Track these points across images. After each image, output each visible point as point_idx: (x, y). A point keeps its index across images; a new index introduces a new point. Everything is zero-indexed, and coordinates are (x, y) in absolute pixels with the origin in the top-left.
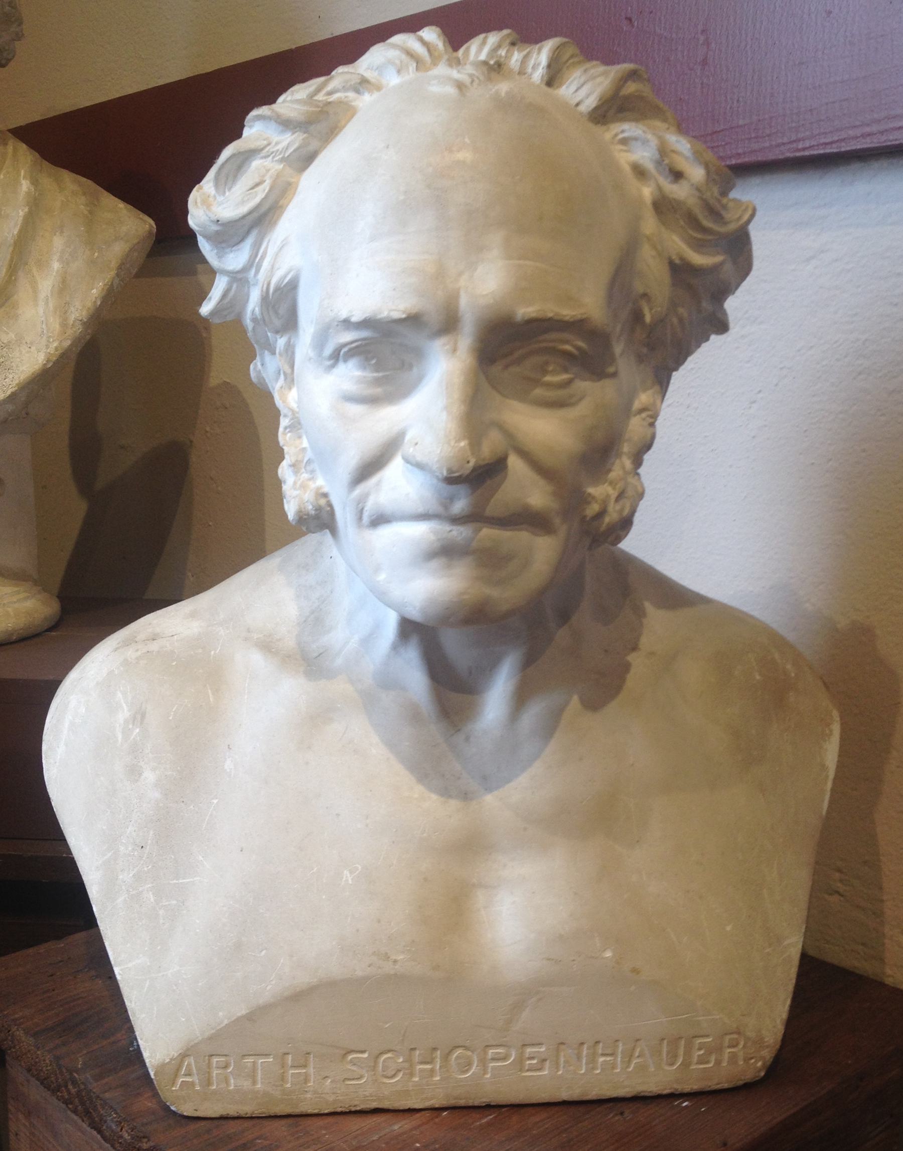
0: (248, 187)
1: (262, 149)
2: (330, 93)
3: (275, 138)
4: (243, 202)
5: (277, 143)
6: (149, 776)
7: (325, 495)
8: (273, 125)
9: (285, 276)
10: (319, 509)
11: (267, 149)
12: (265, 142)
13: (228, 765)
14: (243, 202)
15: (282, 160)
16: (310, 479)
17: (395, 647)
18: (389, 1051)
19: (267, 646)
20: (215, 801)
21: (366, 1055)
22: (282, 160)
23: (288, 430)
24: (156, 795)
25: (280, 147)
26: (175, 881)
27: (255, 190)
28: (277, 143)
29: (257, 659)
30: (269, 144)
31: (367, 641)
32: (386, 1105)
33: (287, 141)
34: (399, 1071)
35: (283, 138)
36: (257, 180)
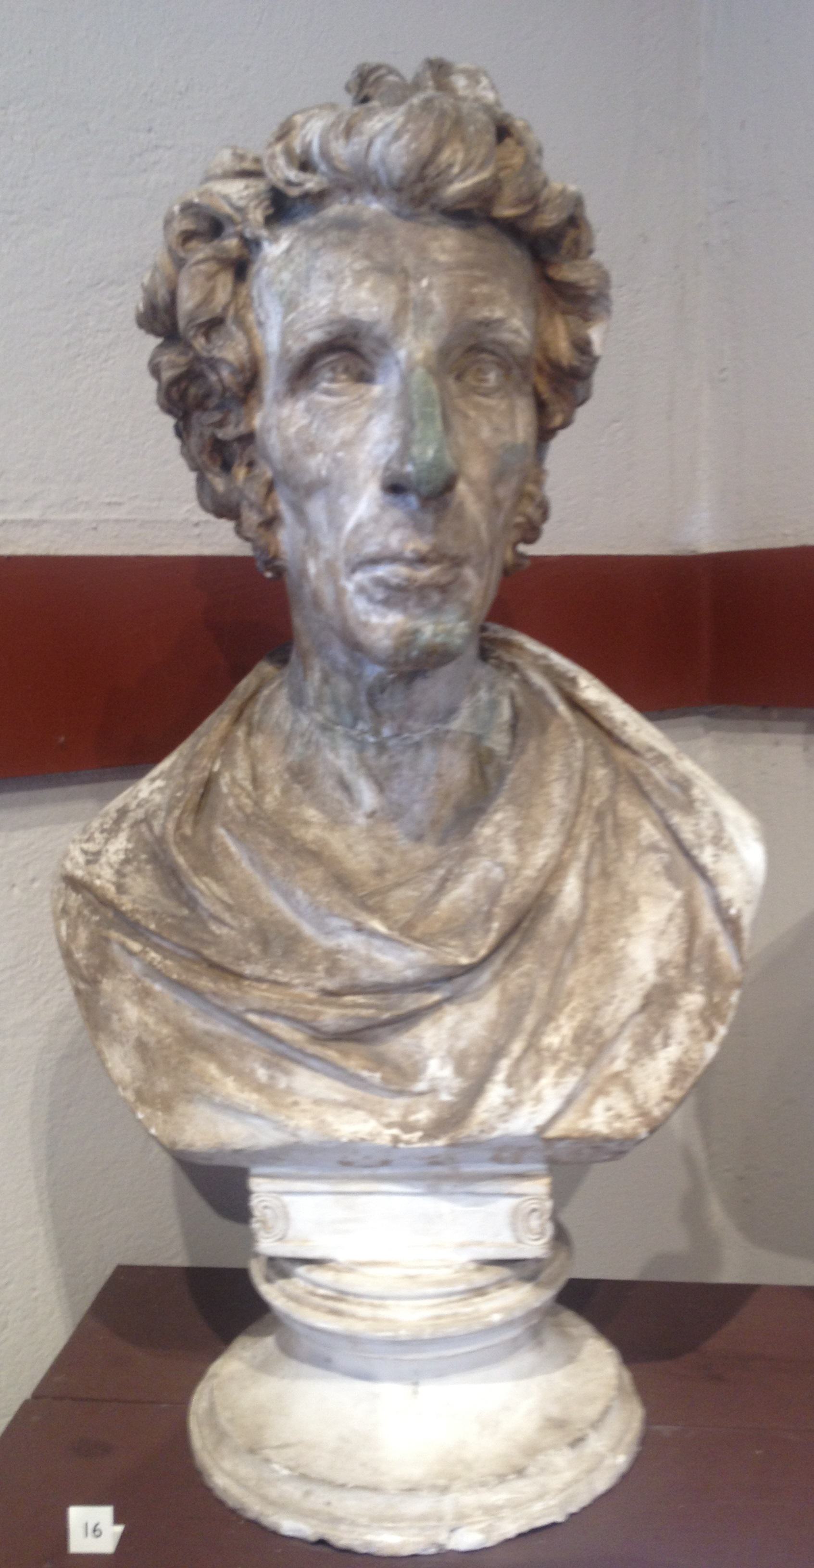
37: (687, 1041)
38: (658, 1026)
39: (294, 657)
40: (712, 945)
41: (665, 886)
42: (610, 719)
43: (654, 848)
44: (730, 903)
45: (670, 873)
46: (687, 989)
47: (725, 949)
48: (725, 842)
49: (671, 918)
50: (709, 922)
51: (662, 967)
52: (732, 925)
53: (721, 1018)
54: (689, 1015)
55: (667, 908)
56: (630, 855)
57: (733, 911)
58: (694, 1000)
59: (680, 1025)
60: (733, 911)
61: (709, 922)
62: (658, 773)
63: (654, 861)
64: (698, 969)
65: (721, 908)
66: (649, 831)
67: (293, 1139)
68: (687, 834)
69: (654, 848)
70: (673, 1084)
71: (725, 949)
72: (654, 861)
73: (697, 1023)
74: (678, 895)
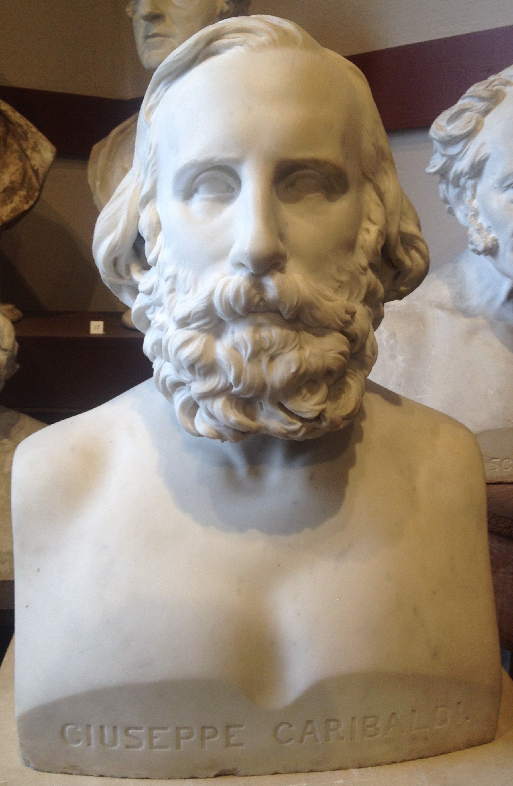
0: (465, 123)
1: (471, 108)
2: (494, 86)
3: (476, 104)
4: (462, 129)
5: (477, 106)
6: (400, 358)
7: (496, 240)
8: (476, 99)
9: (484, 155)
10: (493, 245)
11: (473, 108)
12: (472, 106)
13: (434, 352)
14: (462, 129)
15: (479, 112)
16: (487, 235)
17: (504, 304)
18: (507, 459)
19: (441, 307)
20: (430, 366)
21: (498, 460)
22: (479, 112)
23: (472, 216)
24: (404, 365)
25: (478, 107)
26: (416, 397)
27: (468, 124)
28: (477, 106)
29: (439, 313)
30: (473, 106)
31: (490, 302)
32: (504, 480)
33: (481, 105)
34: (510, 467)
35: (147, 108)
36: (469, 120)
37: (18, 203)
38: (9, 199)
39: (224, 303)
40: (30, 179)
41: (17, 161)
42: (7, 115)
43: (16, 151)
44: (34, 166)
45: (20, 159)
46: (21, 190)
47: (34, 180)
48: (37, 149)
49: (17, 170)
50: (30, 172)
51: (12, 182)
52: (36, 172)
53: (31, 199)
54: (20, 197)
55: (16, 167)
56: (9, 153)
57: (35, 168)
58: (23, 193)
59: (16, 199)
60: (35, 168)
61: (30, 172)
62: (19, 130)
63: (15, 155)
64: (26, 185)
65: (32, 167)
66: (15, 147)
67: (150, 359)
68: (24, 146)
69: (16, 151)
70: (11, 213)
71: (34, 180)
72: (15, 155)
73: (22, 199)
74: (21, 164)
